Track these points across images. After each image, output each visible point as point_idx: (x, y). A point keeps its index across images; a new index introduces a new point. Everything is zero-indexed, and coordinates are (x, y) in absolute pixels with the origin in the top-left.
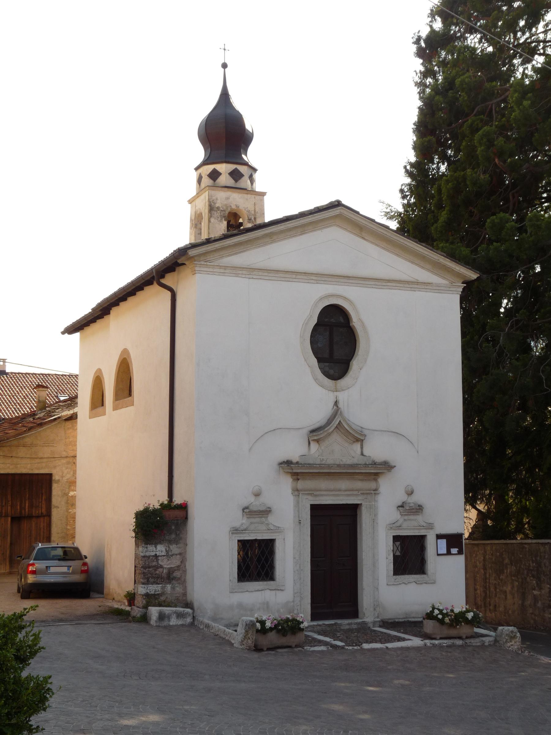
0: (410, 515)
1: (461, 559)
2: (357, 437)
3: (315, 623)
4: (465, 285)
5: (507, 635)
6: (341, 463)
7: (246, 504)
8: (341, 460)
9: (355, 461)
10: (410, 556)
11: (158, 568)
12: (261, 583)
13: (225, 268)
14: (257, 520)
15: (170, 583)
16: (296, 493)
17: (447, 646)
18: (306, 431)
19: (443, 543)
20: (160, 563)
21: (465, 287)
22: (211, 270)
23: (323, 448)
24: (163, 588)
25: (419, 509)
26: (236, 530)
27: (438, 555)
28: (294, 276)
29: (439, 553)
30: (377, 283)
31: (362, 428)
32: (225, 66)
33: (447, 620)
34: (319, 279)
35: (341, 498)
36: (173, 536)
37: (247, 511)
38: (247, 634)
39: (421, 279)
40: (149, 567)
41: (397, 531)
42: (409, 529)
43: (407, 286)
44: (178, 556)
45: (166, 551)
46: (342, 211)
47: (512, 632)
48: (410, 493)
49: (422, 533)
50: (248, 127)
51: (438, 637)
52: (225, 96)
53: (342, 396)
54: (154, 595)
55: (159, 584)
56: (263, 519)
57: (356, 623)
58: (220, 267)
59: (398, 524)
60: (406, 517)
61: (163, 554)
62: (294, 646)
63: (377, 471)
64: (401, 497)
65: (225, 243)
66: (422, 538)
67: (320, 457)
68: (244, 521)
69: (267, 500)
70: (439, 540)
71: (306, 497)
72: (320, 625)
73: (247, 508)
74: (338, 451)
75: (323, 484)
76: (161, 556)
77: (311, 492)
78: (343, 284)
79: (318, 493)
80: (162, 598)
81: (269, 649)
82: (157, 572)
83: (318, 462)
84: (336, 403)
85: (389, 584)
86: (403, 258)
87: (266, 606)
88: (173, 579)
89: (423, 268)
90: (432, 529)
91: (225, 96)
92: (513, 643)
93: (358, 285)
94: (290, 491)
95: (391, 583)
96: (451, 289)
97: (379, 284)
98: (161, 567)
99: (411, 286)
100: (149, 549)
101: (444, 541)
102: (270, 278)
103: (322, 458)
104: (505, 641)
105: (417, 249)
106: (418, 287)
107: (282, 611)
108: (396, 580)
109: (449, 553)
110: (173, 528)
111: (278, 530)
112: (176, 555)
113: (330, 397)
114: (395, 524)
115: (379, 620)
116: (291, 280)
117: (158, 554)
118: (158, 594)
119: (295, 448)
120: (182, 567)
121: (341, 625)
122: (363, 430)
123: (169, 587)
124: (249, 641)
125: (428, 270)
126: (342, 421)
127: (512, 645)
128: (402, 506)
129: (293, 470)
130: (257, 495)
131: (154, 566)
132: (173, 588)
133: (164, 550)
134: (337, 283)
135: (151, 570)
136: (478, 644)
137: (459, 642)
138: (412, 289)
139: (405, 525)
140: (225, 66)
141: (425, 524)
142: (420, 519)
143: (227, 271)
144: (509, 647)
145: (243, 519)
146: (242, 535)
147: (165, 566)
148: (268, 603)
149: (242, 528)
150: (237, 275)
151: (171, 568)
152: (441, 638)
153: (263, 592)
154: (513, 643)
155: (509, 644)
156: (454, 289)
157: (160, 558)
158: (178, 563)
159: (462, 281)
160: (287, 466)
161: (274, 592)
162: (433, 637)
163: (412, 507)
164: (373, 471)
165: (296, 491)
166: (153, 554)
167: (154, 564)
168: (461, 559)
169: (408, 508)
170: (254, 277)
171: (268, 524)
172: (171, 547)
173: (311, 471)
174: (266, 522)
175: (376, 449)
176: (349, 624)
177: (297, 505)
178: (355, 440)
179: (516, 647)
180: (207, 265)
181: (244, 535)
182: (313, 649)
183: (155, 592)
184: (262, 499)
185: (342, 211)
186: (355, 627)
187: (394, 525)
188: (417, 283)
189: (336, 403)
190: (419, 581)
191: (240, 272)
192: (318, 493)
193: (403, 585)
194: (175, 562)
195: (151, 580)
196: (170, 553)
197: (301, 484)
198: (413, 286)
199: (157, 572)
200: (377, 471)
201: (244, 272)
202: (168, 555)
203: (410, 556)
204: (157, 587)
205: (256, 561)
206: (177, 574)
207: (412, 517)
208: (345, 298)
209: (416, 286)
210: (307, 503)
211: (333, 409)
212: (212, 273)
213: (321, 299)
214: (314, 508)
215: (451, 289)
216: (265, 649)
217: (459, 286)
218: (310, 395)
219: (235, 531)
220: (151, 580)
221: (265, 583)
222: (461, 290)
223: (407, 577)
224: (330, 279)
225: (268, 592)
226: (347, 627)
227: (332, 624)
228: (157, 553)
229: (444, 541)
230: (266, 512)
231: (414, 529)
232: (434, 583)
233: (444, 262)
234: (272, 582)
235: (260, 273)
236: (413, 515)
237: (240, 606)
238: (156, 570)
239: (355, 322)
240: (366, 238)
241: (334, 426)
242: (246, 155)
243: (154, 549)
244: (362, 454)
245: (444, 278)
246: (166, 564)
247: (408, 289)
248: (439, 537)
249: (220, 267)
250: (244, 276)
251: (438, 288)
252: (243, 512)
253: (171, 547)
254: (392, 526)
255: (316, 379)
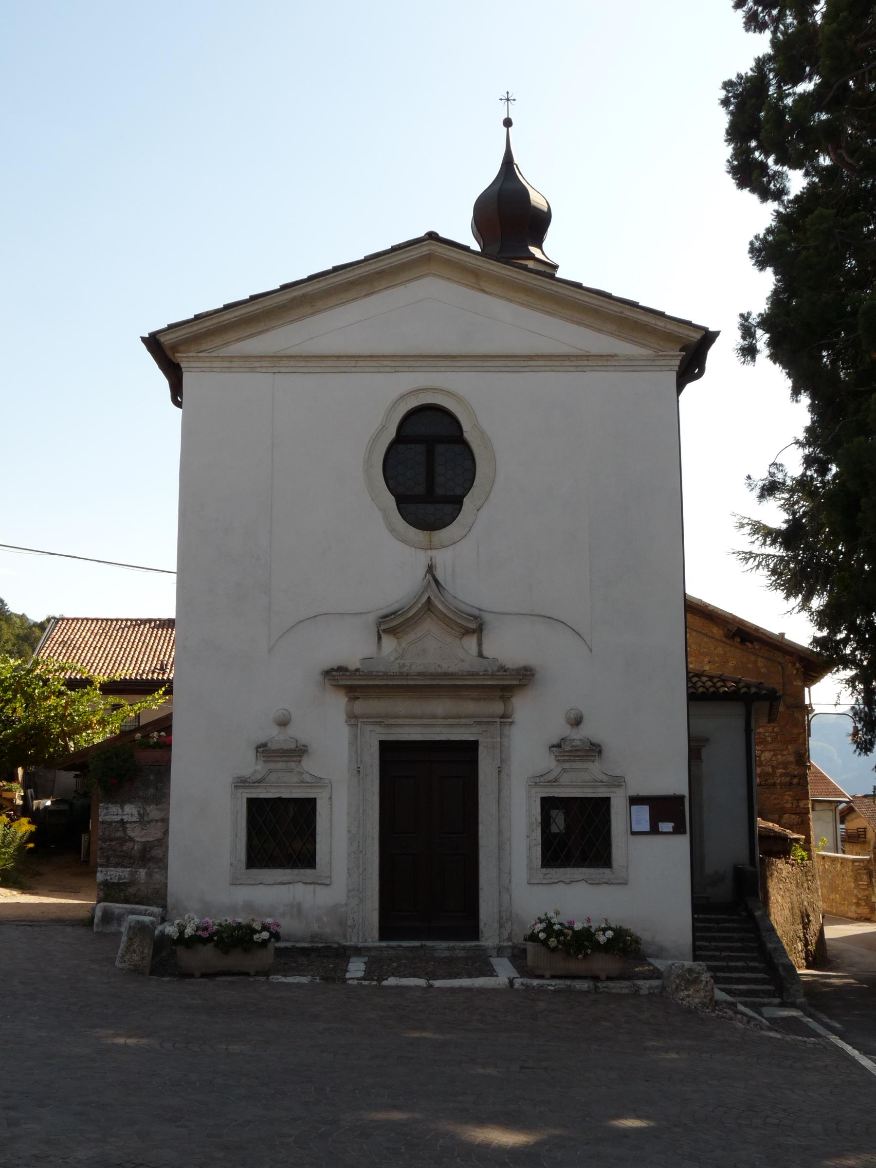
0: (574, 761)
1: (683, 842)
2: (474, 626)
3: (384, 944)
4: (684, 353)
5: (678, 976)
6: (439, 670)
7: (262, 740)
8: (440, 666)
9: (466, 667)
10: (577, 834)
11: (126, 841)
12: (288, 871)
13: (231, 359)
14: (281, 765)
15: (144, 866)
16: (353, 721)
17: (555, 991)
18: (372, 618)
19: (642, 816)
20: (130, 833)
21: (684, 357)
22: (208, 364)
23: (404, 645)
24: (131, 873)
25: (594, 750)
26: (244, 781)
27: (633, 833)
28: (353, 363)
29: (635, 829)
30: (509, 363)
31: (480, 610)
32: (508, 123)
33: (553, 942)
34: (399, 364)
35: (438, 730)
36: (152, 791)
37: (263, 750)
38: (132, 945)
39: (594, 351)
40: (111, 840)
41: (548, 790)
42: (575, 785)
43: (568, 363)
44: (160, 824)
45: (139, 814)
46: (433, 248)
47: (690, 971)
48: (577, 722)
49: (602, 793)
50: (536, 199)
51: (548, 974)
52: (508, 162)
53: (443, 559)
54: (118, 884)
55: (126, 867)
56: (292, 764)
57: (464, 948)
58: (223, 358)
59: (551, 777)
60: (567, 765)
61: (134, 819)
62: (252, 972)
63: (508, 684)
64: (558, 729)
65: (222, 319)
66: (605, 802)
67: (399, 661)
68: (259, 768)
69: (299, 731)
70: (634, 808)
71: (371, 727)
72: (393, 948)
73: (264, 745)
74: (434, 650)
75: (402, 706)
76: (131, 823)
77: (380, 720)
78: (443, 369)
79: (392, 721)
80: (132, 890)
81: (203, 975)
82: (125, 848)
83: (395, 669)
84: (431, 569)
85: (532, 881)
86: (561, 318)
87: (297, 910)
88: (149, 860)
89: (600, 331)
90: (619, 786)
91: (508, 162)
92: (690, 993)
93: (472, 369)
94: (343, 717)
95: (536, 881)
96: (658, 363)
97: (513, 364)
98: (131, 839)
99: (575, 363)
100: (110, 810)
101: (646, 808)
102: (311, 370)
103: (402, 662)
104: (674, 987)
105: (579, 297)
106: (590, 363)
107: (325, 919)
108: (549, 876)
109: (654, 830)
110: (152, 777)
111: (318, 782)
112: (157, 821)
113: (421, 560)
114: (545, 777)
115: (510, 944)
116: (348, 370)
117: (126, 818)
118: (124, 883)
119: (353, 647)
120: (162, 842)
121: (433, 949)
122: (482, 613)
123: (142, 872)
124: (134, 955)
125: (611, 334)
126: (432, 598)
127: (688, 996)
128: (559, 746)
129: (344, 680)
130: (283, 723)
131: (117, 839)
132: (149, 875)
133: (135, 811)
134: (434, 369)
135: (113, 843)
136: (625, 991)
137: (583, 985)
138: (579, 369)
139: (565, 779)
140: (508, 123)
141: (605, 778)
142: (595, 769)
143: (234, 365)
144: (683, 999)
145: (256, 764)
146: (253, 790)
147: (138, 839)
148: (299, 907)
149: (253, 779)
150: (252, 370)
151: (148, 842)
152: (553, 977)
153: (291, 886)
154: (690, 993)
155: (682, 994)
156: (663, 363)
157: (128, 825)
158: (159, 835)
159: (679, 347)
160: (336, 676)
161: (311, 887)
162: (539, 972)
163: (577, 746)
164: (489, 683)
165: (353, 718)
166: (118, 818)
167: (120, 834)
168: (683, 842)
169: (568, 748)
170: (282, 370)
171: (302, 773)
172: (148, 809)
173: (371, 683)
174: (298, 770)
175: (506, 646)
176: (449, 949)
177: (354, 741)
178: (463, 631)
179: (697, 1000)
180: (197, 357)
181: (259, 790)
182: (283, 980)
183: (120, 878)
184: (293, 731)
185: (433, 248)
186: (462, 954)
187: (542, 779)
188: (588, 357)
189: (431, 569)
190: (593, 879)
191: (258, 364)
192: (392, 721)
193: (561, 885)
194: (153, 834)
195: (113, 860)
196: (146, 819)
197: (360, 707)
198: (580, 363)
199: (125, 848)
200: (508, 684)
201: (264, 364)
202: (143, 821)
203: (577, 834)
204: (123, 872)
205: (280, 832)
206: (157, 852)
207: (578, 765)
208: (448, 393)
209: (586, 363)
210: (373, 737)
211: (424, 579)
212: (210, 369)
213: (403, 397)
214: (385, 746)
215: (658, 363)
216: (197, 974)
217: (673, 356)
218: (388, 560)
219: (241, 783)
220: (113, 860)
221: (296, 871)
222: (678, 363)
223: (569, 871)
224: (418, 364)
225: (300, 887)
226: (447, 954)
227: (417, 947)
228: (124, 817)
229: (646, 808)
230: (299, 752)
231: (582, 787)
232: (625, 883)
233: (632, 315)
234: (308, 871)
235: (292, 363)
236: (582, 761)
237: (249, 907)
238: (122, 845)
239: (469, 434)
240: (487, 290)
241: (429, 607)
242: (540, 247)
243: (120, 811)
244: (480, 655)
245: (644, 346)
246: (138, 835)
247: (570, 369)
248: (635, 800)
249: (223, 358)
250: (264, 370)
251: (630, 364)
252: (257, 752)
253: (148, 809)
254: (536, 781)
255: (392, 530)
